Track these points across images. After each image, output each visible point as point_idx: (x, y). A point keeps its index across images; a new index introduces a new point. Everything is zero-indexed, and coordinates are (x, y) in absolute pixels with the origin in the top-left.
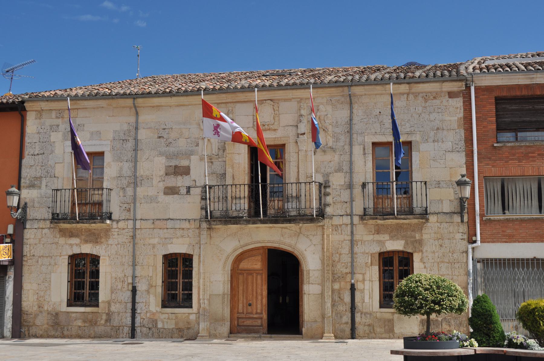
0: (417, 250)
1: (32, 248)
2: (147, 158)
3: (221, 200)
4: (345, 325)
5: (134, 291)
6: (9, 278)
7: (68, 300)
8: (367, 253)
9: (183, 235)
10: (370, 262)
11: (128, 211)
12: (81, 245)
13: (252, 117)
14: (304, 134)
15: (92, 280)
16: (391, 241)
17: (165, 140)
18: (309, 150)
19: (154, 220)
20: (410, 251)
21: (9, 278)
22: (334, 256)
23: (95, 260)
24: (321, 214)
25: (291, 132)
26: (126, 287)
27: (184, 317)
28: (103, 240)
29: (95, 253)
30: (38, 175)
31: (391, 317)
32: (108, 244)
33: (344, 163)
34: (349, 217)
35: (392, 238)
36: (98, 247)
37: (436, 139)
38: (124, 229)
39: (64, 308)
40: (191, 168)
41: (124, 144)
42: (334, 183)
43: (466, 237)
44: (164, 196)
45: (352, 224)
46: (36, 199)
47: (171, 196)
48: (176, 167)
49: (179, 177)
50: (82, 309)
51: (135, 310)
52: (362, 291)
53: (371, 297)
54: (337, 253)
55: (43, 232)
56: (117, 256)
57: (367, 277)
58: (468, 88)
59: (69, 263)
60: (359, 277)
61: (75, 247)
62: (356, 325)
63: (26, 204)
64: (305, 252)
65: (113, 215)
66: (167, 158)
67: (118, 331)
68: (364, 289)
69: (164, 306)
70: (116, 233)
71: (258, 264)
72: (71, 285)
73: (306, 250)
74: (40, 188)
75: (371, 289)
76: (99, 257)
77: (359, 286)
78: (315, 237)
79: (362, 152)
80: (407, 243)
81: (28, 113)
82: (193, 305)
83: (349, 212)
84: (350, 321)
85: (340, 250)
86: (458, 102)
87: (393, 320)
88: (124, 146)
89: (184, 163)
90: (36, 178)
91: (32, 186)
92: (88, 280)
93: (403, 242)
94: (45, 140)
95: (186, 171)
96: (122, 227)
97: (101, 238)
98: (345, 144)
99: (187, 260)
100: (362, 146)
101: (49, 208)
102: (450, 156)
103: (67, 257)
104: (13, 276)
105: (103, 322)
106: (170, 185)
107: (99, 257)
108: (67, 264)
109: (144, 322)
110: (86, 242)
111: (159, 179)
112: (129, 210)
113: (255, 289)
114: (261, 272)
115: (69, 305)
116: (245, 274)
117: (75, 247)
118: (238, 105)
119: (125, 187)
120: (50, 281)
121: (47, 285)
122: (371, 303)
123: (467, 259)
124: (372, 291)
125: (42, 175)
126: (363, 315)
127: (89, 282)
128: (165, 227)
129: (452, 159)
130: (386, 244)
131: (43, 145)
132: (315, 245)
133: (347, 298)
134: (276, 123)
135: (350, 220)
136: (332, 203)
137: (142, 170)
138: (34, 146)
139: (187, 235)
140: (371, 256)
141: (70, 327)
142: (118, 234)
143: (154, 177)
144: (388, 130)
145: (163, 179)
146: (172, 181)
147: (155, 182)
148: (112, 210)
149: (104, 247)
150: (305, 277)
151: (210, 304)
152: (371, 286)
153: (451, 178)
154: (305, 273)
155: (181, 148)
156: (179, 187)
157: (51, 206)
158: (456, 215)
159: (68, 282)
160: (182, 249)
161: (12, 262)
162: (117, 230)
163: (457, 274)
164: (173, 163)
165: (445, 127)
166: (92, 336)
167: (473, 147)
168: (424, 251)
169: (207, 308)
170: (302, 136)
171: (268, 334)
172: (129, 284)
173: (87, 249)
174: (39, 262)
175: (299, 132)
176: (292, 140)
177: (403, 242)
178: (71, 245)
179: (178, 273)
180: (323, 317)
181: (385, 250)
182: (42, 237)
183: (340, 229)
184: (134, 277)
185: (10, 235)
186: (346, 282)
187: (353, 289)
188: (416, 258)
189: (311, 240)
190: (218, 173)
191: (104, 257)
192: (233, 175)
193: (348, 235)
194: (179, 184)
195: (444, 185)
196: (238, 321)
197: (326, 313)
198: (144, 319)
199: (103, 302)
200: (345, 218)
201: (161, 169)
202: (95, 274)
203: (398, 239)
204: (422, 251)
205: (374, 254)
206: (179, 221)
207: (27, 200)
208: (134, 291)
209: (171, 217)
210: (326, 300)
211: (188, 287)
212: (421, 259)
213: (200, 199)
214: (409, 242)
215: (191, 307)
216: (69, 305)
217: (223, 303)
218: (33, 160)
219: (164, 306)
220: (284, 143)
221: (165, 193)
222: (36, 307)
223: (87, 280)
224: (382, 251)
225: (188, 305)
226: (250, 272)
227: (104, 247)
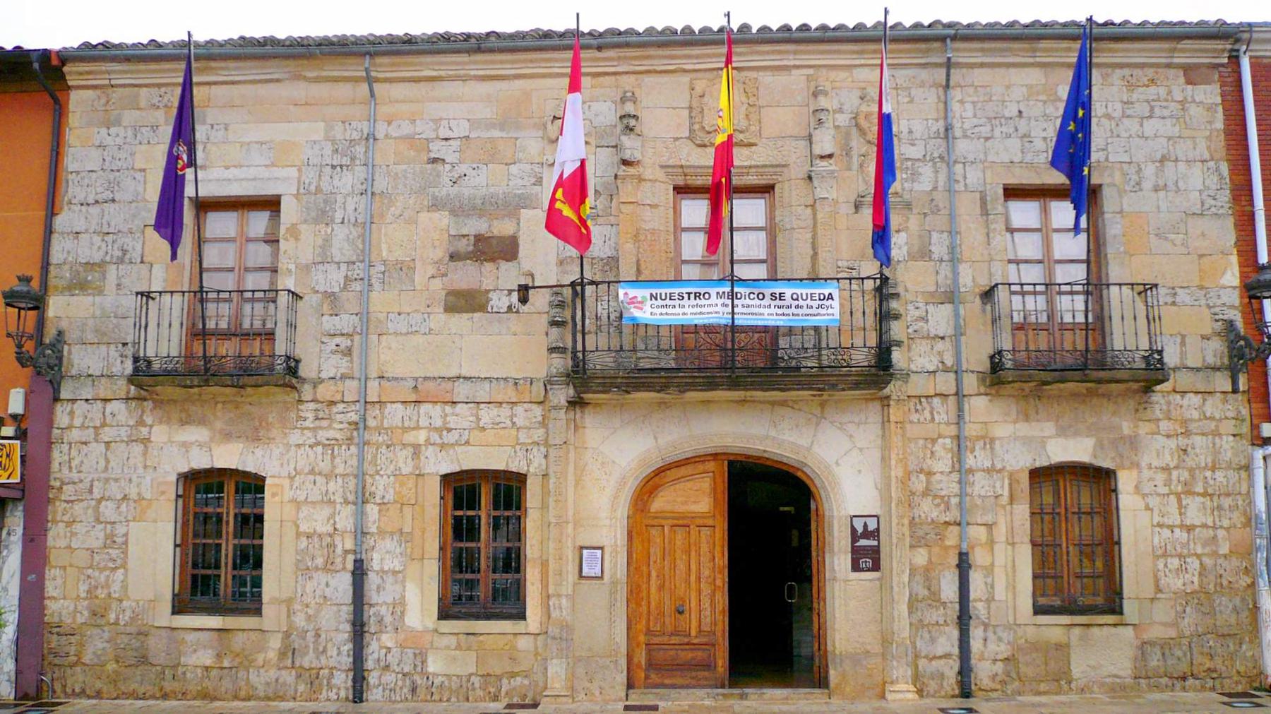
0: (1127, 463)
1: (74, 453)
2: (398, 213)
3: (605, 328)
4: (942, 662)
5: (359, 572)
6: (9, 534)
7: (174, 595)
8: (999, 471)
10: (1006, 493)
11: (345, 355)
12: (213, 445)
13: (686, 112)
14: (830, 156)
15: (243, 541)
16: (1061, 441)
17: (448, 167)
18: (841, 200)
19: (416, 379)
20: (1106, 464)
21: (9, 534)
22: (913, 478)
23: (252, 485)
24: (881, 368)
25: (795, 154)
26: (338, 560)
28: (275, 433)
29: (250, 468)
30: (97, 258)
31: (1064, 640)
32: (288, 446)
33: (935, 235)
34: (952, 375)
35: (1062, 432)
36: (259, 452)
37: (1161, 183)
38: (333, 403)
39: (163, 615)
40: (521, 242)
41: (336, 178)
43: (1245, 429)
44: (443, 317)
45: (959, 395)
46: (91, 322)
47: (466, 316)
48: (479, 238)
49: (489, 266)
50: (214, 621)
51: (363, 625)
52: (989, 570)
53: (1012, 587)
55: (108, 411)
56: (311, 477)
57: (1001, 532)
58: (1235, 59)
59: (178, 496)
60: (977, 533)
61: (195, 451)
62: (973, 662)
63: (60, 333)
64: (836, 469)
65: (301, 366)
66: (453, 212)
67: (317, 682)
68: (992, 564)
69: (444, 615)
70: (310, 416)
71: (700, 499)
72: (184, 554)
73: (837, 463)
74: (100, 291)
75: (1010, 564)
76: (263, 479)
77: (979, 557)
78: (862, 427)
79: (978, 211)
80: (1100, 445)
81: (74, 96)
83: (949, 361)
84: (956, 651)
85: (929, 462)
86: (1210, 94)
87: (1068, 646)
88: (336, 182)
89: (503, 228)
90: (90, 266)
91: (79, 285)
92: (232, 542)
93: (1089, 443)
94: (119, 164)
95: (507, 250)
96: (328, 398)
97: (269, 427)
98: (935, 188)
99: (508, 490)
100: (978, 195)
101: (125, 344)
102: (1197, 226)
103: (174, 478)
104: (20, 531)
105: (272, 655)
106: (463, 286)
107: (263, 479)
108: (174, 496)
109: (389, 657)
110: (227, 436)
111: (431, 270)
112: (348, 352)
113: (693, 567)
115: (179, 607)
116: (666, 529)
117: (195, 451)
118: (649, 79)
119: (336, 290)
120: (126, 543)
121: (114, 553)
122: (1010, 603)
123: (1251, 485)
124: (1014, 571)
125: (108, 259)
126: (990, 634)
128: (448, 398)
129: (1203, 234)
130: (1049, 448)
131: (111, 177)
132: (861, 450)
133: (949, 590)
134: (753, 128)
135: (954, 384)
136: (905, 340)
137: (384, 246)
138: (86, 181)
139: (509, 423)
140: (1010, 479)
141: (180, 670)
142: (317, 419)
143: (418, 264)
145: (443, 271)
146: (468, 276)
147: (419, 279)
148: (299, 352)
149: (276, 452)
152: (1010, 559)
153: (1201, 279)
155: (492, 190)
156: (488, 291)
157: (129, 339)
158: (1218, 373)
159: (176, 546)
160: (496, 460)
161: (22, 486)
162: (312, 406)
163: (1226, 523)
164: (475, 226)
165: (1181, 156)
166: (243, 694)
167: (1252, 205)
168: (1143, 464)
170: (824, 163)
171: (732, 685)
172: (346, 552)
173: (228, 456)
174: (95, 490)
176: (798, 170)
177: (1089, 443)
178: (186, 446)
179: (483, 528)
181: (1046, 464)
182: (104, 425)
183: (928, 409)
184: (361, 533)
185: (15, 417)
186: (946, 548)
187: (964, 565)
188: (1125, 481)
189: (851, 436)
191: (276, 481)
192: (638, 261)
193: (948, 424)
194: (487, 284)
195: (1188, 300)
196: (649, 652)
198: (389, 649)
199: (275, 601)
200: (941, 377)
201: (437, 243)
202: (252, 523)
203: (1077, 434)
204: (1138, 465)
205: (1018, 471)
207: (64, 325)
208: (359, 572)
209: (464, 373)
210: (896, 597)
212: (1136, 487)
214: (1106, 442)
216: (179, 607)
217: (612, 605)
218: (83, 219)
219: (444, 615)
221: (450, 309)
222: (86, 613)
223: (228, 545)
224: (1038, 465)
226: (683, 522)
227: (276, 452)
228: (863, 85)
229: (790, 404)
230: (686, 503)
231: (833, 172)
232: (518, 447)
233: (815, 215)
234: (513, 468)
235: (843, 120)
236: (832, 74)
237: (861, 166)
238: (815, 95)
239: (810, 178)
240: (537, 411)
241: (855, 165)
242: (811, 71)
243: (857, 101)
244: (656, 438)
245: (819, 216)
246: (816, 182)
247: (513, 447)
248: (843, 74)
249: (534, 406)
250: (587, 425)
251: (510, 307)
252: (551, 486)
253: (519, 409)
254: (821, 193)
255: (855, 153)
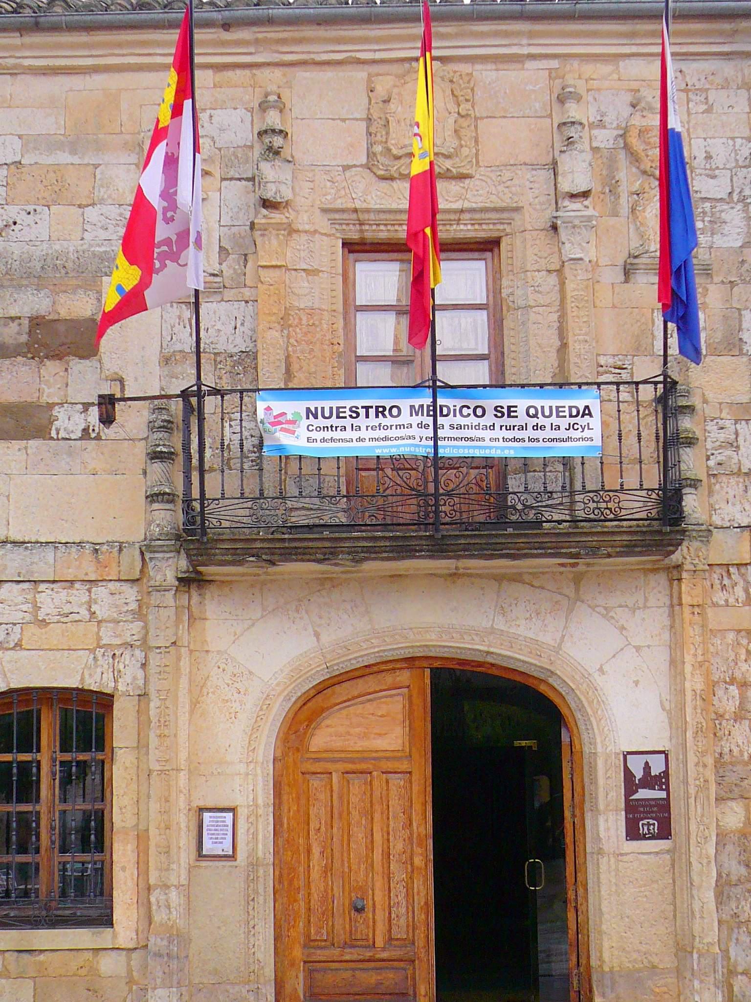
9: (67, 609)
13: (364, 124)
14: (585, 194)
22: (720, 693)
25: (531, 193)
27: (74, 966)
42: (710, 396)
47: (16, 444)
48: (36, 322)
49: (52, 367)
54: (733, 681)
64: (599, 680)
71: (389, 729)
73: (601, 670)
82: (118, 915)
114: (405, 766)
116: (335, 776)
118: (303, 75)
127: (38, 800)
132: (638, 649)
134: (465, 151)
136: (703, 476)
139: (84, 613)
144: (108, 677)
150: (601, 781)
151: (189, 909)
154: (600, 763)
156: (50, 406)
169: (181, 923)
170: (576, 205)
175: (565, 186)
180: (683, 949)
190: (220, 348)
192: (288, 357)
194: (51, 394)
197: (697, 929)
206: (50, 550)
211: (92, 834)
213: (143, 457)
215: (106, 920)
217: (250, 900)
220: (496, 234)
225: (94, 913)
226: (361, 767)
228: (634, 85)
229: (526, 578)
230: (365, 736)
231: (590, 218)
232: (99, 652)
233: (562, 284)
234: (92, 684)
235: (605, 138)
236: (589, 69)
237: (633, 210)
238: (561, 100)
239: (555, 228)
240: (131, 593)
241: (625, 210)
242: (554, 64)
243: (627, 111)
244: (317, 635)
245: (570, 286)
246: (563, 234)
247: (92, 651)
248: (605, 69)
249: (126, 587)
250: (209, 614)
251: (85, 431)
252: (152, 713)
253: (100, 592)
254: (571, 251)
255: (624, 190)
